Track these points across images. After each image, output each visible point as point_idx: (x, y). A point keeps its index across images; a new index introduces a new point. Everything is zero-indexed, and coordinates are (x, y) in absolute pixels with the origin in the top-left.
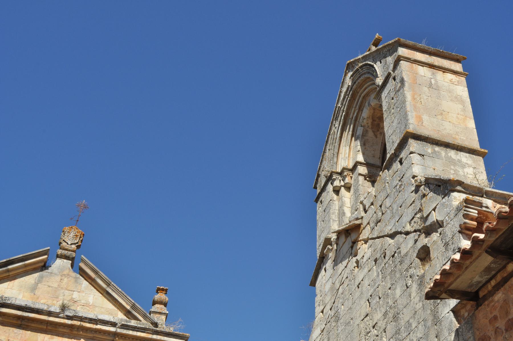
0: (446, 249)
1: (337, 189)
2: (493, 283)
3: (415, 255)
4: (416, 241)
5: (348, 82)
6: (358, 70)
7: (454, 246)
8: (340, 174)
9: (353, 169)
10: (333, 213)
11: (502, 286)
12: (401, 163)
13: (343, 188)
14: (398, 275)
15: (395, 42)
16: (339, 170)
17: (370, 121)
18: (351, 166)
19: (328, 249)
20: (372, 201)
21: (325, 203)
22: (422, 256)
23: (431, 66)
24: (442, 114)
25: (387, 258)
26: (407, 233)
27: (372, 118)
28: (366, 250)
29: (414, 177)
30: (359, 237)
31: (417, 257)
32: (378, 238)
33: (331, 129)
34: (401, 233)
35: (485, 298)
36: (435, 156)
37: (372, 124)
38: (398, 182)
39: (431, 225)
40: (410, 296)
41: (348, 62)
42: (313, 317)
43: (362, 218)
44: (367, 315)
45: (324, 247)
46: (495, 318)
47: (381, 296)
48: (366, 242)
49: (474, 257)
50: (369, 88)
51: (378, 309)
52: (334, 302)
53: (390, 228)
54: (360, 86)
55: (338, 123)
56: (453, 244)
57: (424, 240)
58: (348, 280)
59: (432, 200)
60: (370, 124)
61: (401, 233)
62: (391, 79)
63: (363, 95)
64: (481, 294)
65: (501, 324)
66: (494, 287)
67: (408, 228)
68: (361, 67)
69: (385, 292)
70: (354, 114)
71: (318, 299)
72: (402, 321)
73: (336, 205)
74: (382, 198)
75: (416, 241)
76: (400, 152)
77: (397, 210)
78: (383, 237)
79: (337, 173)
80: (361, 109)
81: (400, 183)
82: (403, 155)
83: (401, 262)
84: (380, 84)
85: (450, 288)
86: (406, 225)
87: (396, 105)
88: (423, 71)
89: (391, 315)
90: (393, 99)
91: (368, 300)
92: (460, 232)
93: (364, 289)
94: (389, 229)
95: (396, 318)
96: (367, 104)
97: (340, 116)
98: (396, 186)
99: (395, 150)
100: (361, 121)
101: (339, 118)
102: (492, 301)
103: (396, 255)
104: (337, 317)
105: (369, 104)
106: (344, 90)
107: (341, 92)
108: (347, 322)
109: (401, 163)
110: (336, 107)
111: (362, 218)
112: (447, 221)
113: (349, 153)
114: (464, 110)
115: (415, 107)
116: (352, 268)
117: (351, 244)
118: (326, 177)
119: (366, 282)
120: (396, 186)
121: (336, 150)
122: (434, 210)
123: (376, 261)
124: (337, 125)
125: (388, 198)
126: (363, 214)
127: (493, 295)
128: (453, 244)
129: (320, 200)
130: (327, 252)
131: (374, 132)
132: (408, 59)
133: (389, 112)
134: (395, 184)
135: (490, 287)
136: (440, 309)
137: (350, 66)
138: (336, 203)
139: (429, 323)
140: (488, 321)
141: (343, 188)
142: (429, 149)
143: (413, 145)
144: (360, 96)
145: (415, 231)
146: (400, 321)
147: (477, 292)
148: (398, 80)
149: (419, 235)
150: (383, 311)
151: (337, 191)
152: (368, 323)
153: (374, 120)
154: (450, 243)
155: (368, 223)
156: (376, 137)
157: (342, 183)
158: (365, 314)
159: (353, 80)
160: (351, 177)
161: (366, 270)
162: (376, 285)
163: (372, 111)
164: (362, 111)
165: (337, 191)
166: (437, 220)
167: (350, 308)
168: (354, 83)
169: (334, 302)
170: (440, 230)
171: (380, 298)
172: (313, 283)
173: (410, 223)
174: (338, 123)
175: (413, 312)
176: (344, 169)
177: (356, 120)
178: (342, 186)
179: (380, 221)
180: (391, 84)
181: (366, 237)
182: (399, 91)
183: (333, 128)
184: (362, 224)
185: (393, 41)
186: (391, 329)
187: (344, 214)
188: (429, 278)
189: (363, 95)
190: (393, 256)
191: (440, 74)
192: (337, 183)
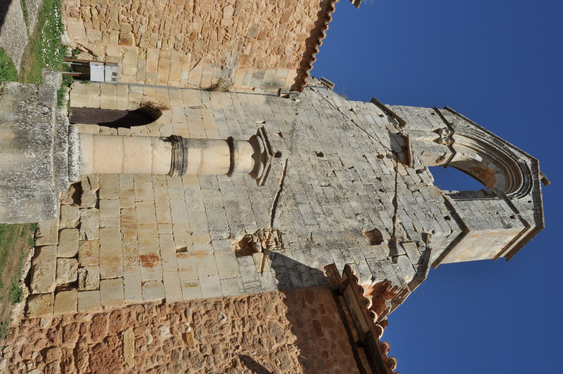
0: (377, 264)
1: (440, 132)
2: (347, 312)
3: (377, 228)
4: (387, 229)
5: (523, 159)
6: (530, 173)
7: (377, 273)
8: (451, 137)
9: (451, 147)
10: (422, 127)
11: (343, 322)
12: (447, 218)
13: (439, 137)
14: (366, 205)
15: (542, 223)
16: (454, 136)
17: (484, 168)
18: (455, 146)
19: (397, 123)
20: (425, 181)
21: (431, 118)
22: (375, 232)
23: (511, 243)
24: (473, 247)
25: (379, 193)
26: (394, 219)
27: (485, 170)
28: (389, 169)
29: (433, 232)
30: (401, 162)
31: (376, 229)
32: (396, 183)
33: (488, 133)
34: (395, 212)
35: (338, 302)
36: (443, 243)
37: (481, 169)
38: (433, 212)
39: (395, 248)
40: (350, 218)
41: (538, 162)
42: (350, 98)
43: (413, 168)
44: (343, 165)
45: (399, 120)
46: (323, 312)
47: (354, 183)
48: (396, 169)
49: (367, 317)
50: (511, 177)
51: (345, 179)
52: (357, 126)
53: (401, 199)
54: (515, 169)
55: (492, 141)
56: (379, 272)
57: (386, 238)
58: (370, 143)
59: (414, 254)
60: (481, 167)
61: (395, 212)
62: (514, 213)
63: (507, 168)
64: (341, 298)
65: (319, 316)
66: (344, 312)
67: (398, 221)
68: (531, 178)
69: (356, 189)
70: (494, 156)
71: (361, 104)
72: (333, 206)
73: (428, 130)
74: (424, 194)
75: (387, 229)
76: (455, 219)
77: (413, 210)
78: (396, 191)
79: (452, 134)
80: (496, 162)
81: (432, 216)
82: (453, 221)
83: (374, 210)
84: (512, 201)
85: (349, 286)
86: (400, 219)
87: (492, 217)
88: (510, 238)
89: (340, 194)
90: (497, 213)
91: (353, 167)
92: (386, 280)
93: (362, 163)
94: (401, 201)
95: (337, 199)
96: (498, 169)
97: (496, 144)
98: (431, 211)
99: (457, 214)
100: (487, 160)
101: (495, 143)
102: (335, 310)
103: (381, 204)
104: (345, 128)
105: (498, 172)
106: (516, 153)
107: (516, 149)
108: (341, 140)
109: (447, 218)
110: (504, 142)
111: (413, 168)
112: (396, 267)
113: (464, 149)
114: (469, 257)
115: (485, 234)
116: (379, 150)
117: (396, 151)
118: (452, 124)
119: (366, 166)
120: (431, 211)
121: (470, 135)
122: (406, 254)
123: (379, 179)
124: (488, 139)
125: (423, 200)
126: (416, 169)
127: (339, 311)
128: (379, 272)
129: (435, 113)
130: (395, 121)
131: (475, 168)
132: (524, 231)
133: (488, 207)
134: (433, 210)
135: (344, 308)
136: (336, 250)
137: (535, 164)
138: (430, 130)
139: (329, 238)
140: (323, 303)
141: (439, 137)
142: (450, 241)
143: (457, 231)
144: (506, 165)
145: (394, 228)
146: (334, 203)
147: (343, 295)
148: (511, 222)
149: (390, 234)
150: (344, 185)
151: (438, 131)
152: (337, 165)
153: (483, 171)
154: (380, 270)
155: (408, 174)
156: (470, 168)
157: (443, 137)
158: (344, 163)
159: (522, 164)
160: (445, 145)
161: (375, 167)
162: (362, 178)
163: (491, 172)
164: (494, 164)
165: (438, 131)
166: (398, 256)
167: (350, 145)
168: (520, 164)
169: (357, 126)
170: (390, 258)
171: (353, 181)
172: (374, 101)
173: (401, 223)
174: (492, 141)
175: (338, 220)
176: (453, 141)
177: (489, 156)
178: (441, 136)
179: (408, 188)
180: (509, 212)
181: (398, 170)
182: (502, 222)
183: (489, 136)
184: (409, 167)
185: (542, 206)
186: (330, 192)
187: (419, 136)
188: (359, 241)
189: (507, 168)
190: (380, 200)
191: (503, 246)
192: (444, 132)
